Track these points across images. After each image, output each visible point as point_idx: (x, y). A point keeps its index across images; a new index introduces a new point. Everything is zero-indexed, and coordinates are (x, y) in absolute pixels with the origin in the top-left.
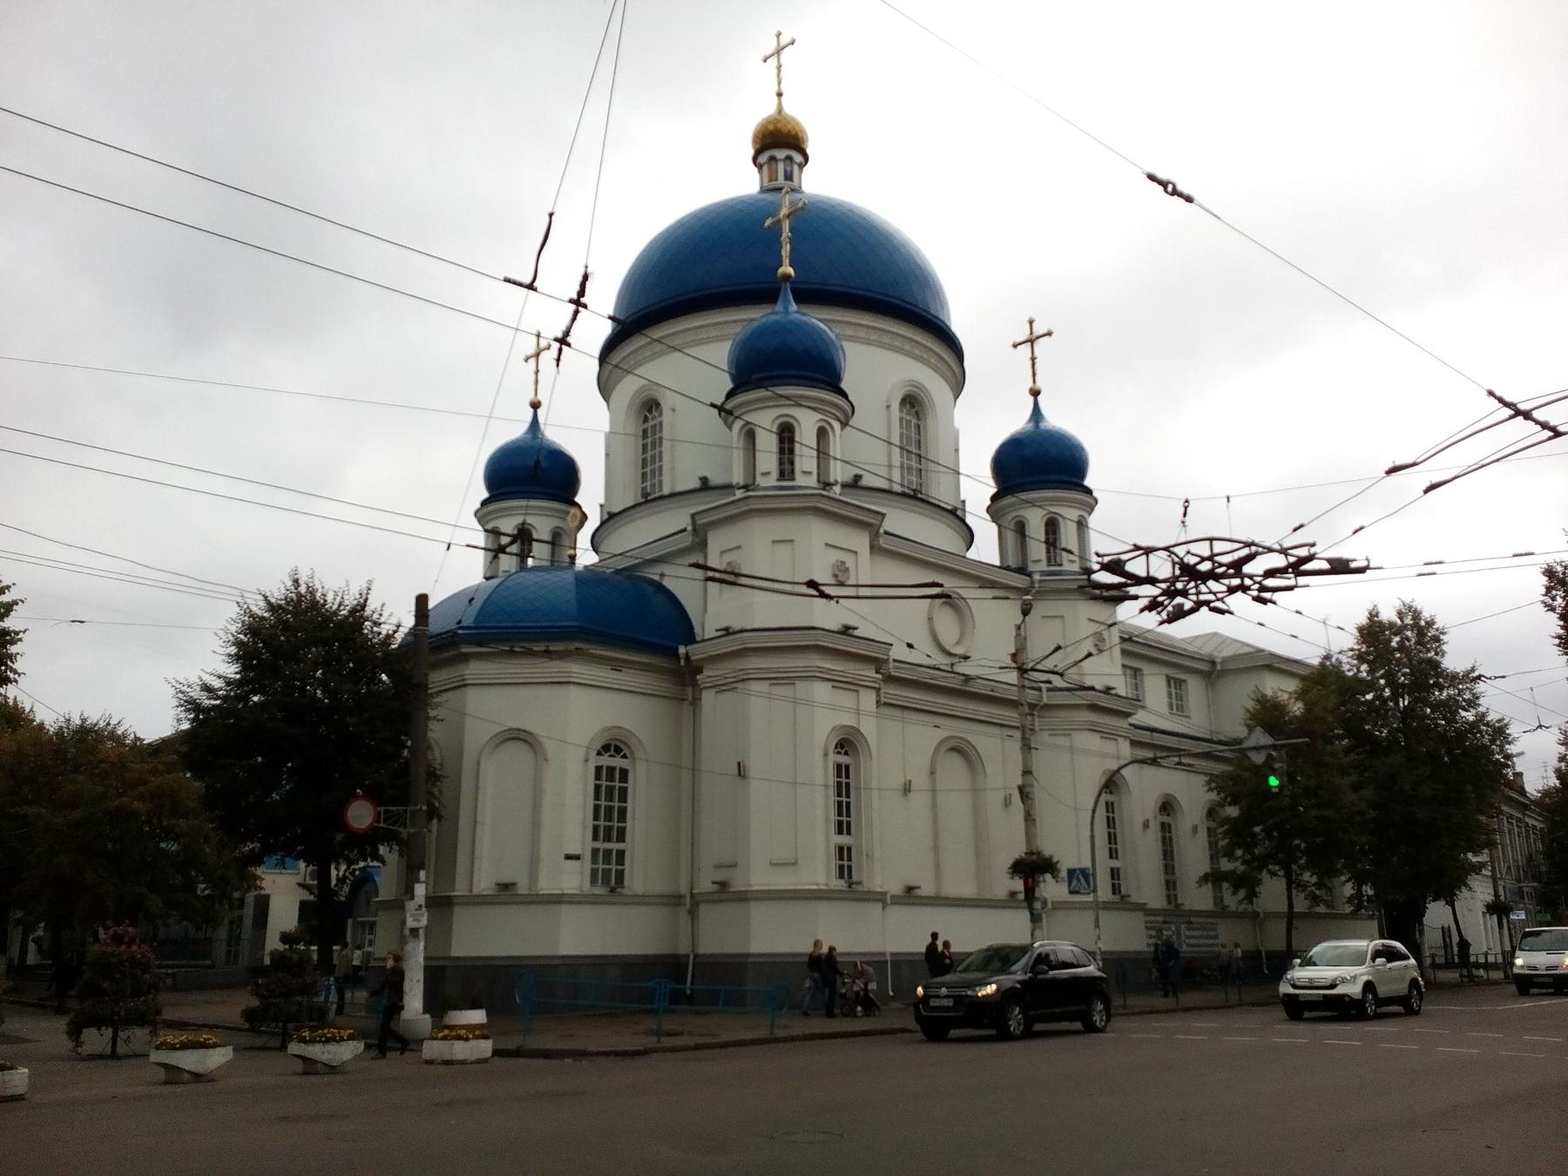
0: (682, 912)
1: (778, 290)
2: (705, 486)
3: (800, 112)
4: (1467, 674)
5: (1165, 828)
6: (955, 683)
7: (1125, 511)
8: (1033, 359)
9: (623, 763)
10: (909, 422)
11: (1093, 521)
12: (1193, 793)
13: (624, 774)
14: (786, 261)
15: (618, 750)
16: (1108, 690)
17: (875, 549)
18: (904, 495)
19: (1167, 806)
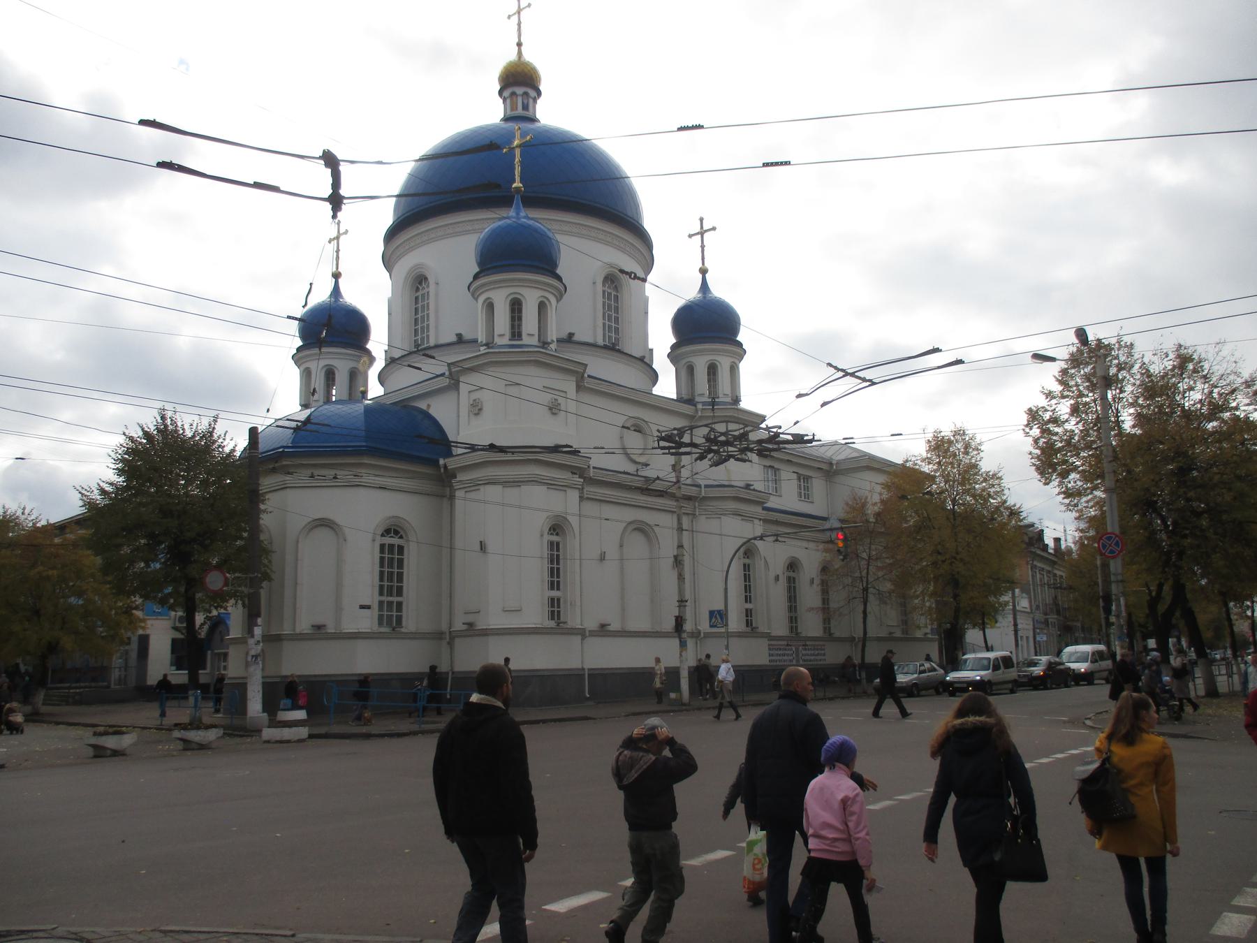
0: (444, 643)
1: (520, 197)
2: (460, 340)
3: (531, 56)
4: (994, 475)
5: (791, 580)
8: (703, 247)
10: (610, 294)
12: (811, 557)
13: (401, 549)
14: (517, 178)
15: (396, 532)
17: (580, 388)
18: (605, 347)
19: (793, 565)
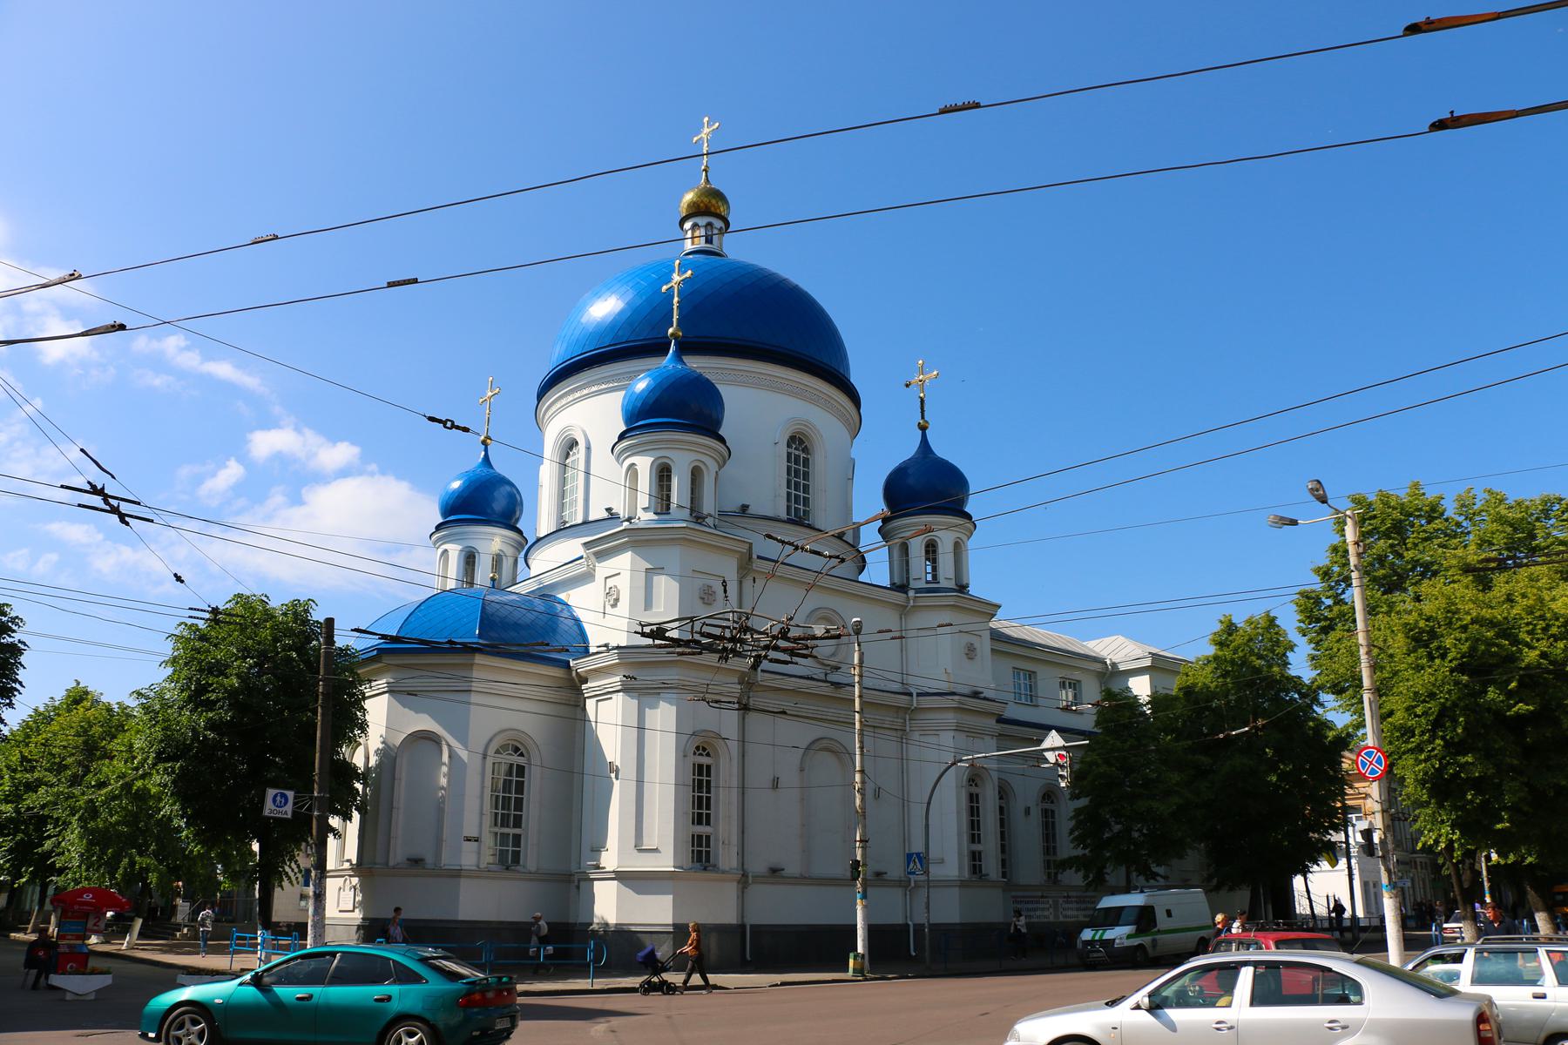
9: (521, 761)
11: (971, 544)
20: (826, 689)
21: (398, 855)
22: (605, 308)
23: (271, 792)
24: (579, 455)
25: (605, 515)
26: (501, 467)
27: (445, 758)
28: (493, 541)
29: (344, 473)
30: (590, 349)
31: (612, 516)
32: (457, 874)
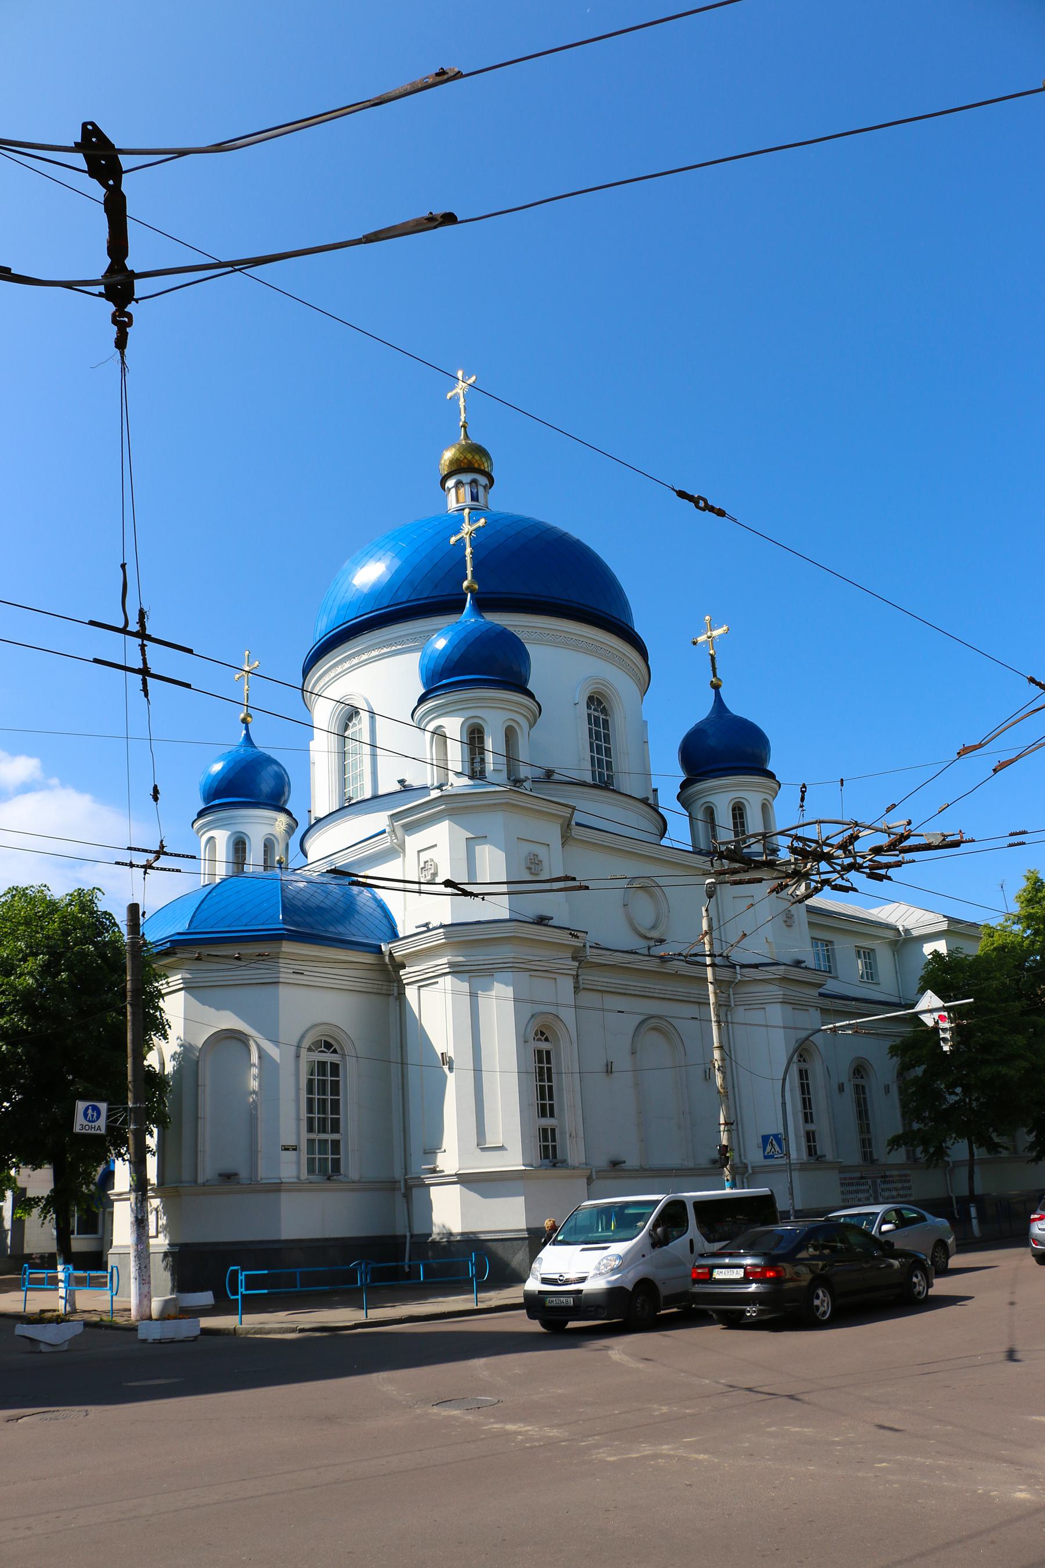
5: (860, 1089)
6: (653, 965)
7: (807, 791)
10: (597, 718)
13: (335, 1067)
16: (798, 964)
17: (566, 838)
20: (653, 965)
21: (208, 1171)
22: (371, 573)
23: (81, 1106)
24: (361, 726)
25: (398, 787)
26: (264, 744)
27: (255, 1058)
28: (262, 825)
29: (26, 788)
30: (351, 616)
31: (405, 788)
32: (277, 1188)
